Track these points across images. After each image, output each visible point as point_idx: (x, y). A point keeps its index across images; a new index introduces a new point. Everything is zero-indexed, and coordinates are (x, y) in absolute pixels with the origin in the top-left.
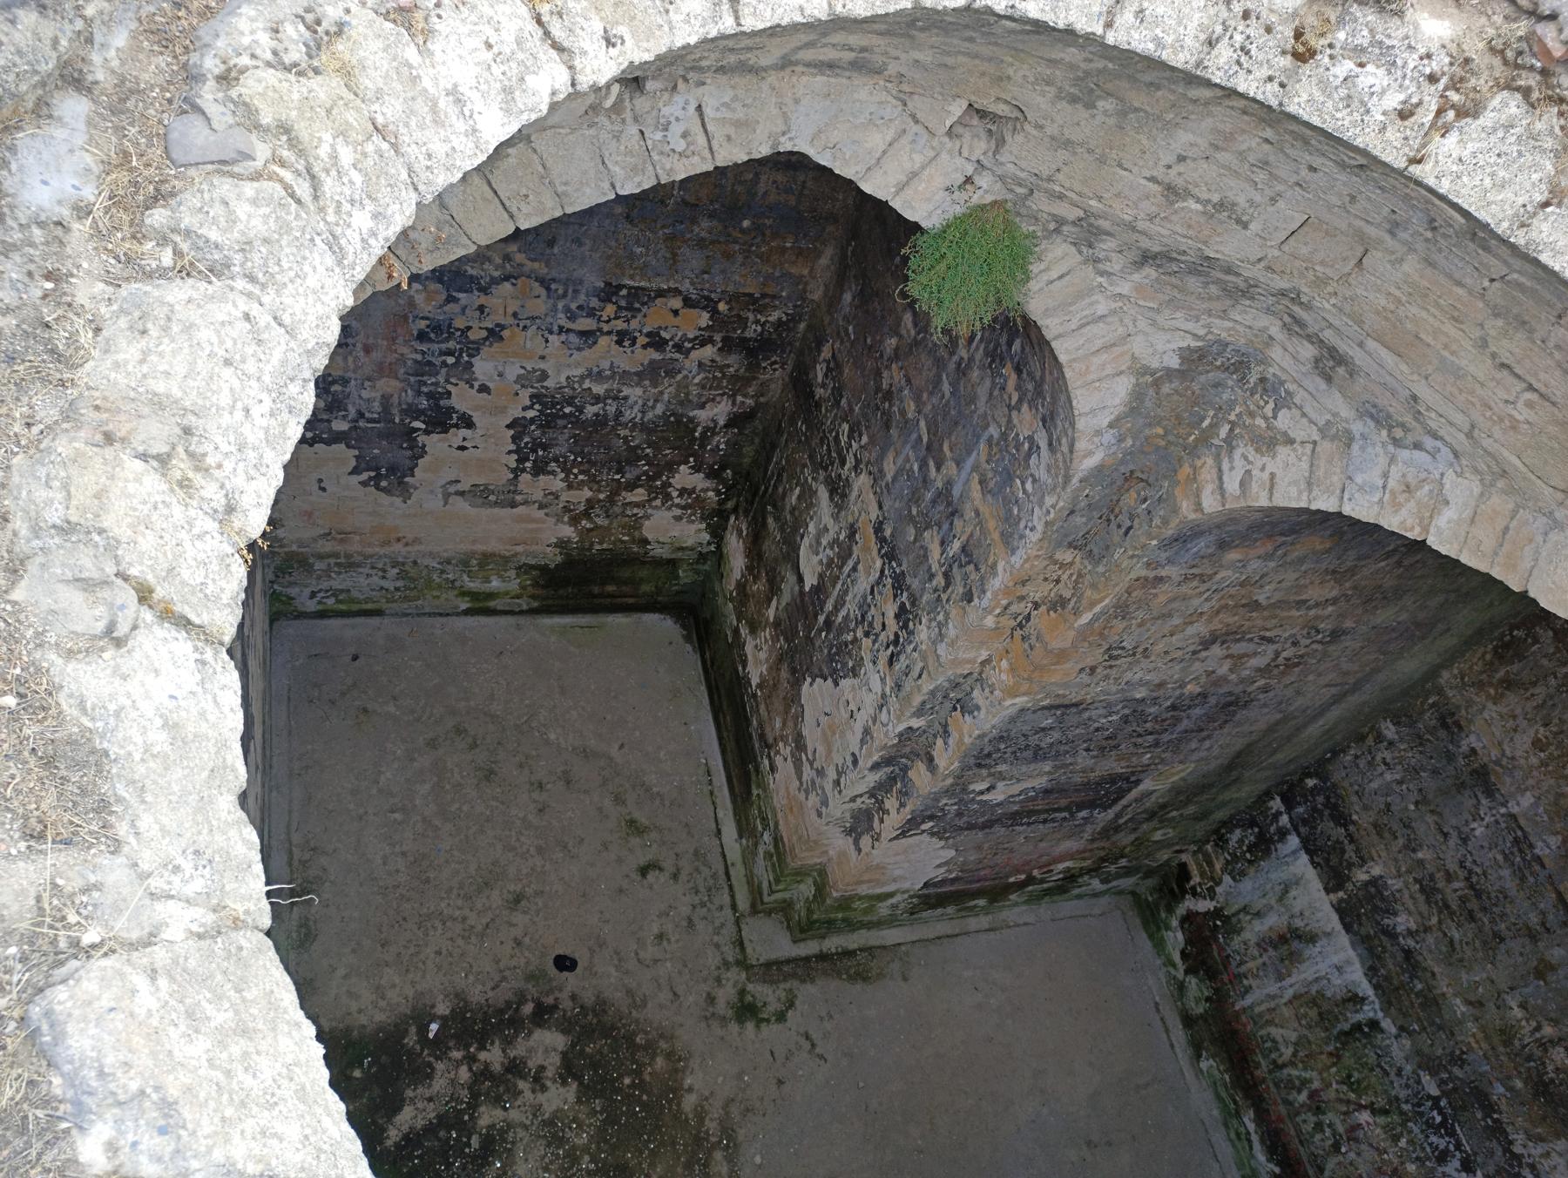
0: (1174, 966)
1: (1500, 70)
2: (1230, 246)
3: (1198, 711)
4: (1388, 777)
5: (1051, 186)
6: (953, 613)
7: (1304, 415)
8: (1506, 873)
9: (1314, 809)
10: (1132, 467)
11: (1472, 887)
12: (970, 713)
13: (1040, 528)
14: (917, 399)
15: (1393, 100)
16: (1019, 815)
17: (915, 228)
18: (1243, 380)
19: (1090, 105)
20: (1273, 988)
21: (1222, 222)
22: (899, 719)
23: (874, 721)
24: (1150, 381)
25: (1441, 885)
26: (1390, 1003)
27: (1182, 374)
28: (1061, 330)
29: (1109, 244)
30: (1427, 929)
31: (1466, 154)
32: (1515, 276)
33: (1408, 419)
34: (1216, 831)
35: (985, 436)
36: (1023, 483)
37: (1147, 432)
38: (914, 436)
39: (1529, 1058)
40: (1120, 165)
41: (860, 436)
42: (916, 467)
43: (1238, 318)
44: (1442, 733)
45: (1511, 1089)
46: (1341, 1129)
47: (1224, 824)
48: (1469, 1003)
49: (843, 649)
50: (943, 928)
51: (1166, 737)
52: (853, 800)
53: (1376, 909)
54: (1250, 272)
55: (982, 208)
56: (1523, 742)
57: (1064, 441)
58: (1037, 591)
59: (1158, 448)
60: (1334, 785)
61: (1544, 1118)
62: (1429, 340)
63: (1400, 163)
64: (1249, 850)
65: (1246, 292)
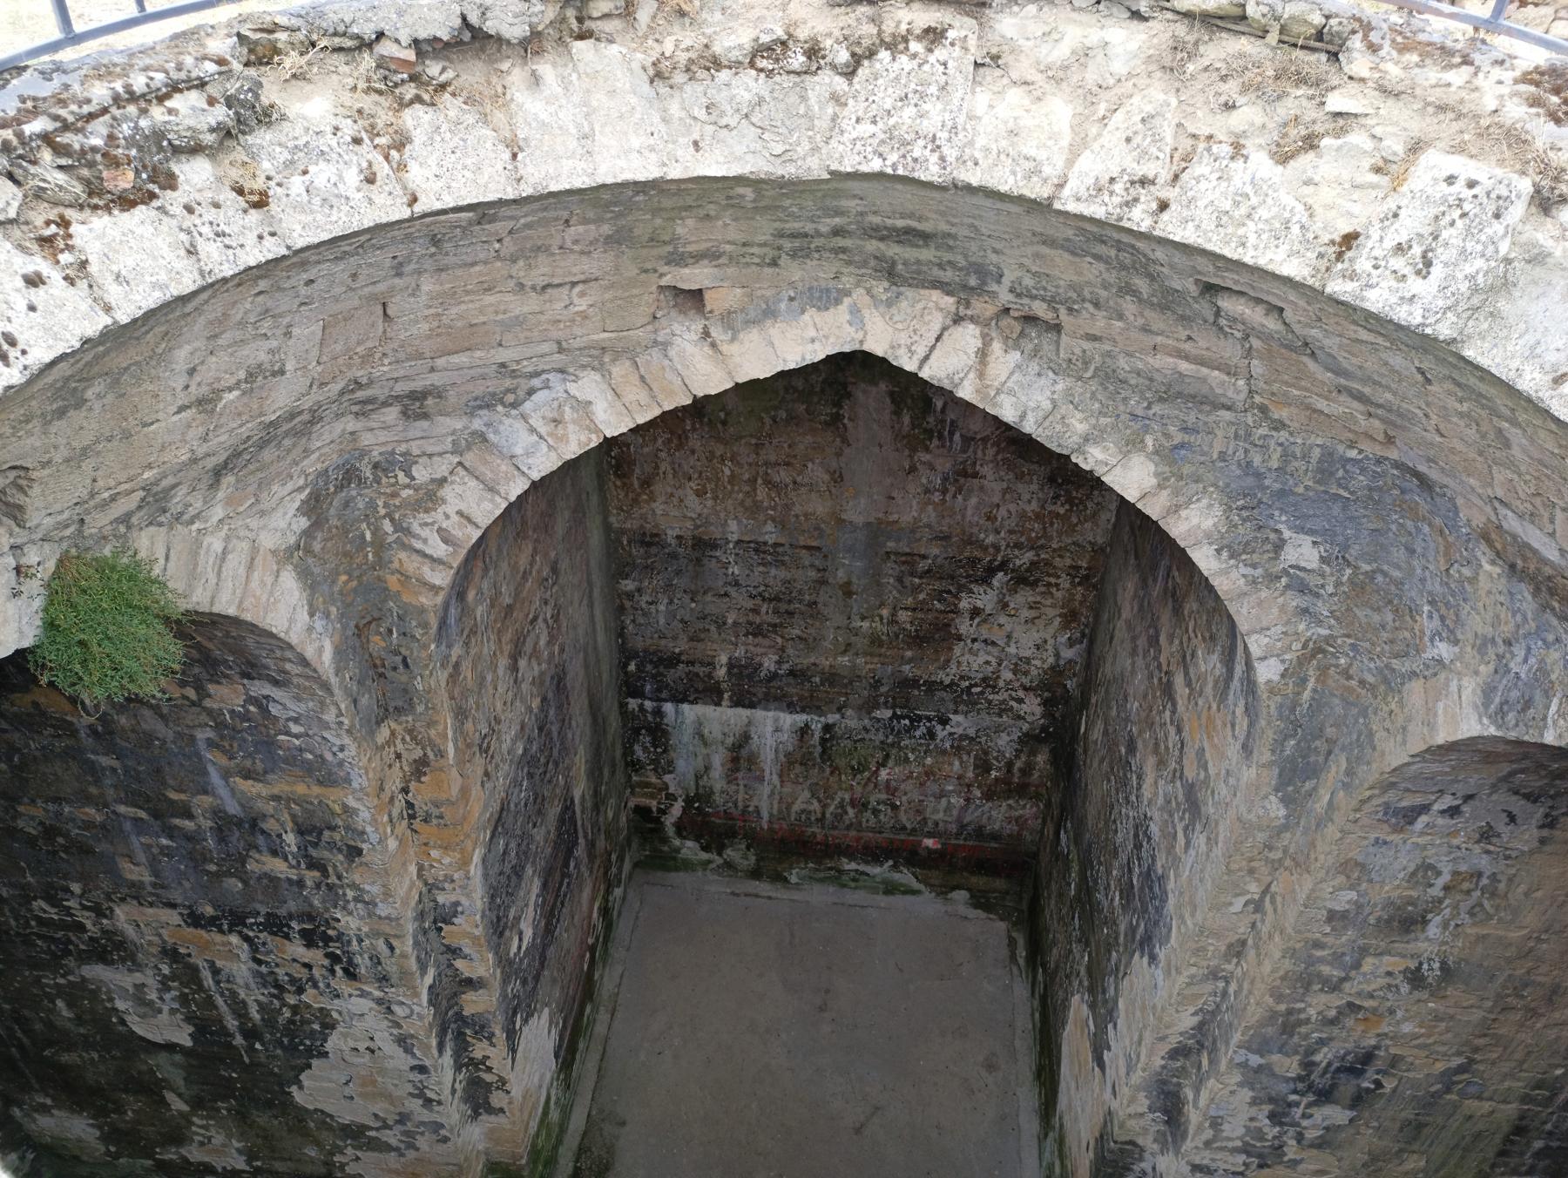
0: (709, 862)
1: (385, 101)
2: (281, 397)
3: (552, 712)
4: (662, 608)
5: (98, 499)
6: (357, 878)
7: (430, 456)
8: (773, 571)
9: (654, 677)
10: (352, 624)
11: (771, 600)
12: (455, 914)
13: (347, 741)
14: (88, 799)
15: (353, 177)
16: (547, 931)
17: (20, 654)
18: (361, 482)
19: (80, 403)
20: (766, 790)
21: (261, 388)
22: (416, 995)
23: (399, 1026)
24: (298, 555)
25: (758, 621)
26: (819, 708)
27: (316, 525)
28: (209, 594)
29: (181, 493)
30: (783, 649)
31: (435, 170)
32: (522, 221)
33: (508, 383)
34: (627, 764)
35: (202, 746)
36: (288, 733)
37: (336, 589)
38: (128, 826)
39: (897, 636)
40: (145, 425)
41: (67, 890)
42: (164, 841)
43: (319, 444)
44: (654, 550)
45: (910, 661)
46: (884, 796)
47: (624, 755)
48: (844, 652)
49: (293, 1029)
50: (591, 1065)
51: (555, 752)
52: (454, 1091)
53: (750, 677)
54: (307, 403)
55: (57, 575)
56: (692, 501)
57: (288, 666)
58: (394, 783)
59: (355, 590)
60: (645, 651)
61: (936, 651)
62: (482, 319)
63: (406, 213)
64: (656, 747)
65: (315, 417)
